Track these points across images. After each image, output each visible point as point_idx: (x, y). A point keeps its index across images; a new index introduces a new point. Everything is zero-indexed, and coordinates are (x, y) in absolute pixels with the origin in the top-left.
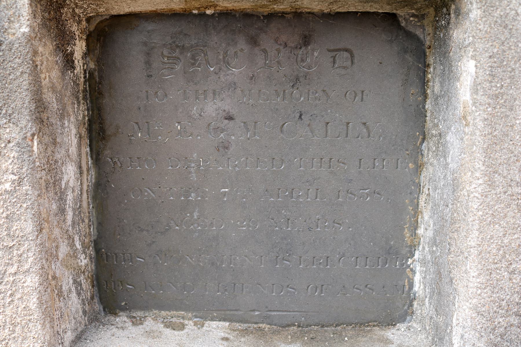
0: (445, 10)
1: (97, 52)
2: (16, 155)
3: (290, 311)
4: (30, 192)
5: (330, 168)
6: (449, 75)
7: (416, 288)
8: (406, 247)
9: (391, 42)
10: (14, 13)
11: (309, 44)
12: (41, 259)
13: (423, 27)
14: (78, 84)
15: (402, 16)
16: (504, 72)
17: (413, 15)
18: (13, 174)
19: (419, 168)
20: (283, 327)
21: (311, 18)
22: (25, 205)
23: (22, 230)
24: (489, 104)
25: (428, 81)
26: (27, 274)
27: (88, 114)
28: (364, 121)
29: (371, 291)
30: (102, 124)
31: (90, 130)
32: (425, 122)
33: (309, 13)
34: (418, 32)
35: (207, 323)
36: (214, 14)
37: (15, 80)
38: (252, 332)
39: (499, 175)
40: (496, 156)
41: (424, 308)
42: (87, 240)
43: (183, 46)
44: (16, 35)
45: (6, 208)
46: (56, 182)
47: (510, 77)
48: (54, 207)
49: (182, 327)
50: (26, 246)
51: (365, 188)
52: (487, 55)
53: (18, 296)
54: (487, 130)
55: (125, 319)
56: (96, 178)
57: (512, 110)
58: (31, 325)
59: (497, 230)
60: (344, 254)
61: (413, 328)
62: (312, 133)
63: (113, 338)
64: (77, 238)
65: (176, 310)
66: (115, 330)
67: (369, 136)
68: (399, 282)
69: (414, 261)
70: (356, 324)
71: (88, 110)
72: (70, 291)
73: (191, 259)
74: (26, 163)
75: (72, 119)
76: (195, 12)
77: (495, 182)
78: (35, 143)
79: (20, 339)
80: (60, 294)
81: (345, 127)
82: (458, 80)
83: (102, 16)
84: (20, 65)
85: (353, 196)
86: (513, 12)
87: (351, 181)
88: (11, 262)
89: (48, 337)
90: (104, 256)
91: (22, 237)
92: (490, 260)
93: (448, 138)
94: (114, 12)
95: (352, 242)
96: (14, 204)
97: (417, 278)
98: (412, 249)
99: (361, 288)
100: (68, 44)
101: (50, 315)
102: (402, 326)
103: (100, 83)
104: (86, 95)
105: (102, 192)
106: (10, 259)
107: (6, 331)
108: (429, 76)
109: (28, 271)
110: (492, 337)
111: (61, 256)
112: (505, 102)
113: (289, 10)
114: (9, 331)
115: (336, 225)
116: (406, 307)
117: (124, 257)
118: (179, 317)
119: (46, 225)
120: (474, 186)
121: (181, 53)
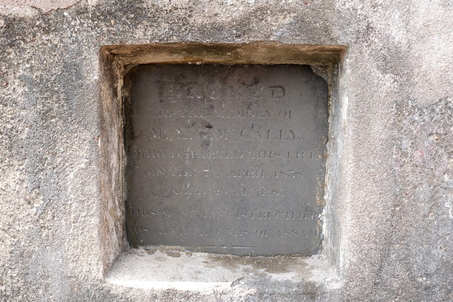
0: (336, 65)
1: (130, 86)
3: (245, 247)
4: (95, 169)
5: (270, 157)
6: (338, 105)
7: (324, 233)
8: (317, 206)
9: (307, 82)
11: (258, 83)
13: (326, 73)
14: (119, 106)
15: (313, 67)
17: (321, 66)
19: (325, 158)
20: (241, 256)
21: (259, 68)
22: (92, 177)
23: (90, 191)
25: (330, 106)
27: (124, 123)
28: (291, 129)
30: (132, 129)
31: (124, 133)
32: (328, 130)
33: (258, 64)
34: (324, 76)
35: (194, 254)
36: (201, 64)
37: (89, 105)
38: (222, 259)
41: (327, 245)
42: (121, 201)
43: (182, 83)
46: (109, 163)
48: (107, 179)
49: (179, 256)
51: (292, 170)
52: (354, 94)
53: (86, 229)
54: (355, 136)
55: (143, 251)
56: (128, 163)
59: (362, 193)
60: (279, 211)
63: (136, 260)
64: (116, 199)
65: (175, 245)
66: (137, 256)
67: (294, 138)
68: (313, 229)
69: (322, 215)
70: (287, 255)
71: (124, 121)
72: (113, 230)
75: (116, 127)
76: (190, 63)
78: (100, 141)
80: (108, 231)
81: (279, 133)
82: (342, 107)
83: (133, 64)
84: (93, 97)
86: (369, 71)
87: (283, 166)
89: (102, 255)
90: (131, 211)
91: (90, 195)
93: (338, 140)
94: (141, 63)
96: (86, 176)
97: (324, 226)
99: (290, 232)
100: (115, 83)
101: (103, 241)
102: (315, 257)
103: (131, 105)
104: (123, 112)
105: (130, 171)
107: (79, 250)
108: (330, 103)
110: (360, 255)
111: (109, 208)
112: (365, 121)
113: (246, 63)
115: (274, 193)
116: (318, 245)
119: (103, 189)
120: (348, 168)
121: (181, 88)
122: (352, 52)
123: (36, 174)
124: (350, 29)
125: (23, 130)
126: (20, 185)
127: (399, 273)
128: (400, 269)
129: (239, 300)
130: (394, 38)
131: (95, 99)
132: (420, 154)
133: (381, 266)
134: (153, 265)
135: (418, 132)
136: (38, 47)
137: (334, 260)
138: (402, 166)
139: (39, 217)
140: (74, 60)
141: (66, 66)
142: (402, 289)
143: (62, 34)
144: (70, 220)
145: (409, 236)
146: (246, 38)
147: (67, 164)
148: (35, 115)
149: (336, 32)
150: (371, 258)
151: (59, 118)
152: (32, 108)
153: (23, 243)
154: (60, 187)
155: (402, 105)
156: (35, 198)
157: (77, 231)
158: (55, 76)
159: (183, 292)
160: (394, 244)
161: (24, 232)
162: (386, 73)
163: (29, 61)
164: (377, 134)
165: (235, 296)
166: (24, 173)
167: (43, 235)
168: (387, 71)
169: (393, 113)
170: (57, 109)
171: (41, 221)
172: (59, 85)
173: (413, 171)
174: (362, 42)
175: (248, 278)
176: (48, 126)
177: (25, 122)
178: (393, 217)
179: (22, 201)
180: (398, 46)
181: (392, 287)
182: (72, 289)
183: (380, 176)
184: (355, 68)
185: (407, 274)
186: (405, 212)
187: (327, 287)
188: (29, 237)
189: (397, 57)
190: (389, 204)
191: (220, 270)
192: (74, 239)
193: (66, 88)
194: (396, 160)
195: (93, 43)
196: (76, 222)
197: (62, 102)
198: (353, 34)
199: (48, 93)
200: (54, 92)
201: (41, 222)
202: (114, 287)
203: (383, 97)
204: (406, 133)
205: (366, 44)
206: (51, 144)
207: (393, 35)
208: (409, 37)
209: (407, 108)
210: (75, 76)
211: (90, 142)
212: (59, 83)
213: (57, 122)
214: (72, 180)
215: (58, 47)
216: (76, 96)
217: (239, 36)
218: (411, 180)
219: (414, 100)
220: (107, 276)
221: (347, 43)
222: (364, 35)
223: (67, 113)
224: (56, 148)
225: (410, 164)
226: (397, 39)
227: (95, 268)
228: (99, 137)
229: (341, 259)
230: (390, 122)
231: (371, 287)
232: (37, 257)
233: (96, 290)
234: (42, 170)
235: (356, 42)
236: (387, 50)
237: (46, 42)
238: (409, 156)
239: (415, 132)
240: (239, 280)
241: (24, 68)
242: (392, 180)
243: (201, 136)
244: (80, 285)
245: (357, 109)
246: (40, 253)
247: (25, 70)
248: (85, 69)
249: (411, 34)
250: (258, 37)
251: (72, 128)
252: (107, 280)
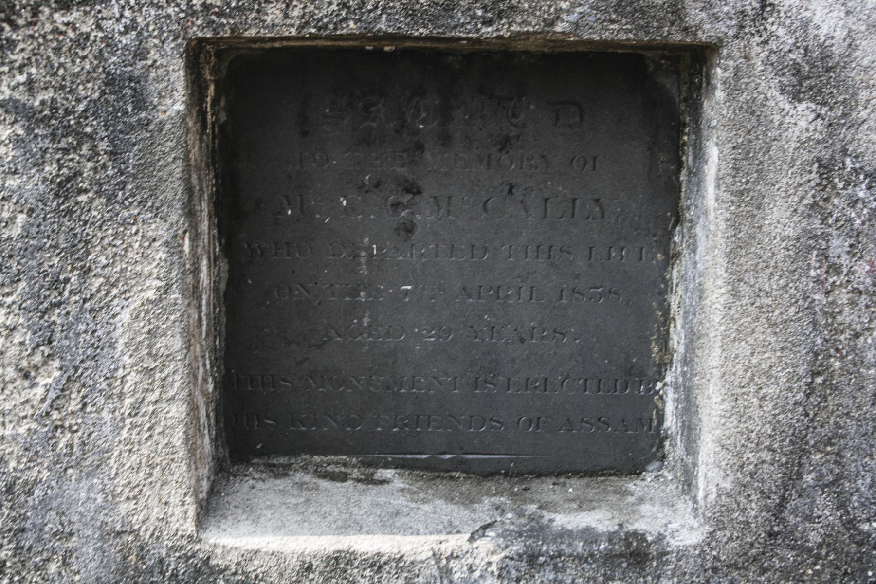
2: (164, 256)
4: (179, 301)
6: (700, 156)
8: (654, 366)
10: (166, 87)
12: (189, 383)
16: (749, 164)
18: (158, 279)
19: (671, 258)
22: (172, 318)
24: (732, 202)
26: (171, 402)
28: (596, 196)
29: (606, 426)
32: (680, 198)
39: (745, 283)
40: (741, 262)
41: (675, 450)
44: (168, 114)
45: (149, 320)
47: (757, 171)
50: (172, 367)
51: (598, 285)
52: (730, 145)
54: (731, 232)
57: (760, 209)
58: (173, 465)
59: (743, 349)
61: (665, 477)
62: (527, 212)
65: (336, 454)
66: (251, 482)
67: (603, 216)
68: (645, 414)
73: (358, 381)
74: (176, 267)
77: (739, 292)
79: (159, 484)
81: (570, 205)
82: (706, 162)
84: (172, 149)
85: (581, 297)
86: (762, 96)
87: (577, 277)
88: (151, 388)
91: (168, 356)
92: (736, 384)
95: (579, 359)
96: (157, 318)
98: (663, 366)
99: (592, 421)
106: (151, 384)
107: (141, 474)
109: (173, 398)
110: (739, 475)
112: (751, 199)
114: (145, 474)
115: (557, 335)
116: (654, 449)
117: (263, 379)
118: (339, 463)
120: (715, 296)
122: (728, 57)
123: (44, 313)
124: (726, 9)
125: (12, 219)
126: (7, 338)
127: (820, 513)
128: (824, 507)
129: (486, 570)
130: (818, 27)
131: (179, 152)
132: (868, 268)
133: (783, 499)
134: (294, 501)
135: (863, 223)
136: (44, 37)
137: (688, 484)
138: (828, 293)
139: (51, 406)
140: (129, 68)
141: (111, 82)
142: (829, 545)
143: (100, 12)
144: (122, 411)
145: (844, 437)
146: (503, 25)
147: (115, 291)
148: (42, 188)
149: (695, 15)
150: (763, 481)
151: (96, 192)
152: (33, 171)
153: (12, 464)
154: (99, 340)
155: (831, 167)
156: (40, 365)
157: (138, 434)
158: (85, 103)
159: (369, 555)
160: (810, 453)
161: (14, 439)
162: (800, 101)
163: (25, 68)
164: (776, 227)
165: (477, 561)
166: (17, 312)
167: (61, 445)
168: (802, 96)
169: (812, 184)
170: (92, 173)
171: (55, 415)
172: (95, 123)
173: (853, 303)
174: (749, 35)
175: (503, 523)
176: (69, 212)
177: (17, 202)
178: (808, 398)
179: (11, 373)
180: (827, 44)
181: (808, 541)
182: (125, 558)
183: (781, 313)
184: (733, 88)
185: (839, 514)
186: (834, 388)
187: (672, 541)
188: (26, 449)
189: (823, 67)
190: (801, 370)
191: (439, 507)
192: (130, 451)
193: (111, 128)
194: (818, 281)
195: (170, 31)
196: (136, 414)
197: (103, 158)
198: (731, 18)
199: (70, 139)
200: (81, 137)
201: (54, 417)
202: (219, 551)
203: (791, 150)
204: (839, 224)
205: (757, 39)
206: (77, 250)
207: (817, 20)
208: (850, 25)
209: (841, 172)
210: (133, 102)
211: (167, 243)
212: (96, 119)
213: (91, 201)
214: (126, 325)
215: (92, 38)
216: (134, 145)
217: (488, 22)
218: (848, 320)
219: (857, 157)
220: (202, 528)
221: (719, 38)
222: (754, 20)
223: (113, 182)
224: (90, 257)
225: (846, 288)
226: (824, 30)
227: (178, 511)
228: (185, 232)
229: (701, 483)
230: (806, 202)
231: (761, 541)
232: (46, 494)
233: (179, 557)
234: (58, 305)
235: (736, 37)
236: (802, 51)
237: (63, 28)
238: (845, 273)
239: (858, 222)
240: (485, 528)
241: (13, 84)
242: (806, 321)
243: (395, 211)
244: (142, 549)
245: (734, 177)
246: (53, 483)
247: (13, 89)
248: (153, 88)
249: (855, 19)
250: (530, 24)
251: (126, 214)
252: (203, 536)
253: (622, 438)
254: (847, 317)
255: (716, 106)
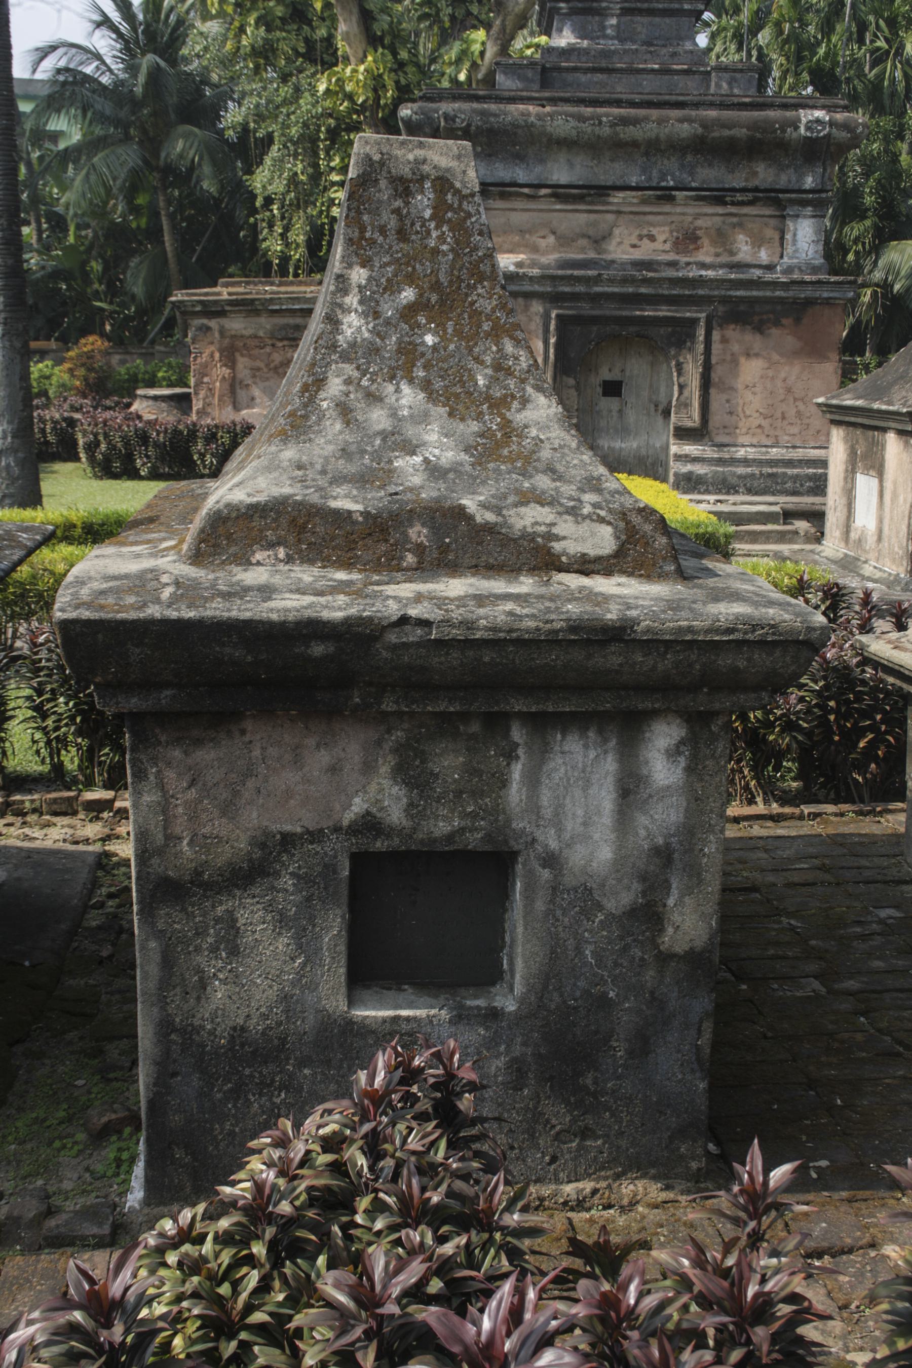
19: (505, 910)
41: (507, 977)
59: (529, 946)
98: (503, 947)
137: (512, 990)
141: (326, 866)
184: (524, 865)
206: (311, 919)
253: (491, 975)
254: (562, 935)
255: (519, 867)
